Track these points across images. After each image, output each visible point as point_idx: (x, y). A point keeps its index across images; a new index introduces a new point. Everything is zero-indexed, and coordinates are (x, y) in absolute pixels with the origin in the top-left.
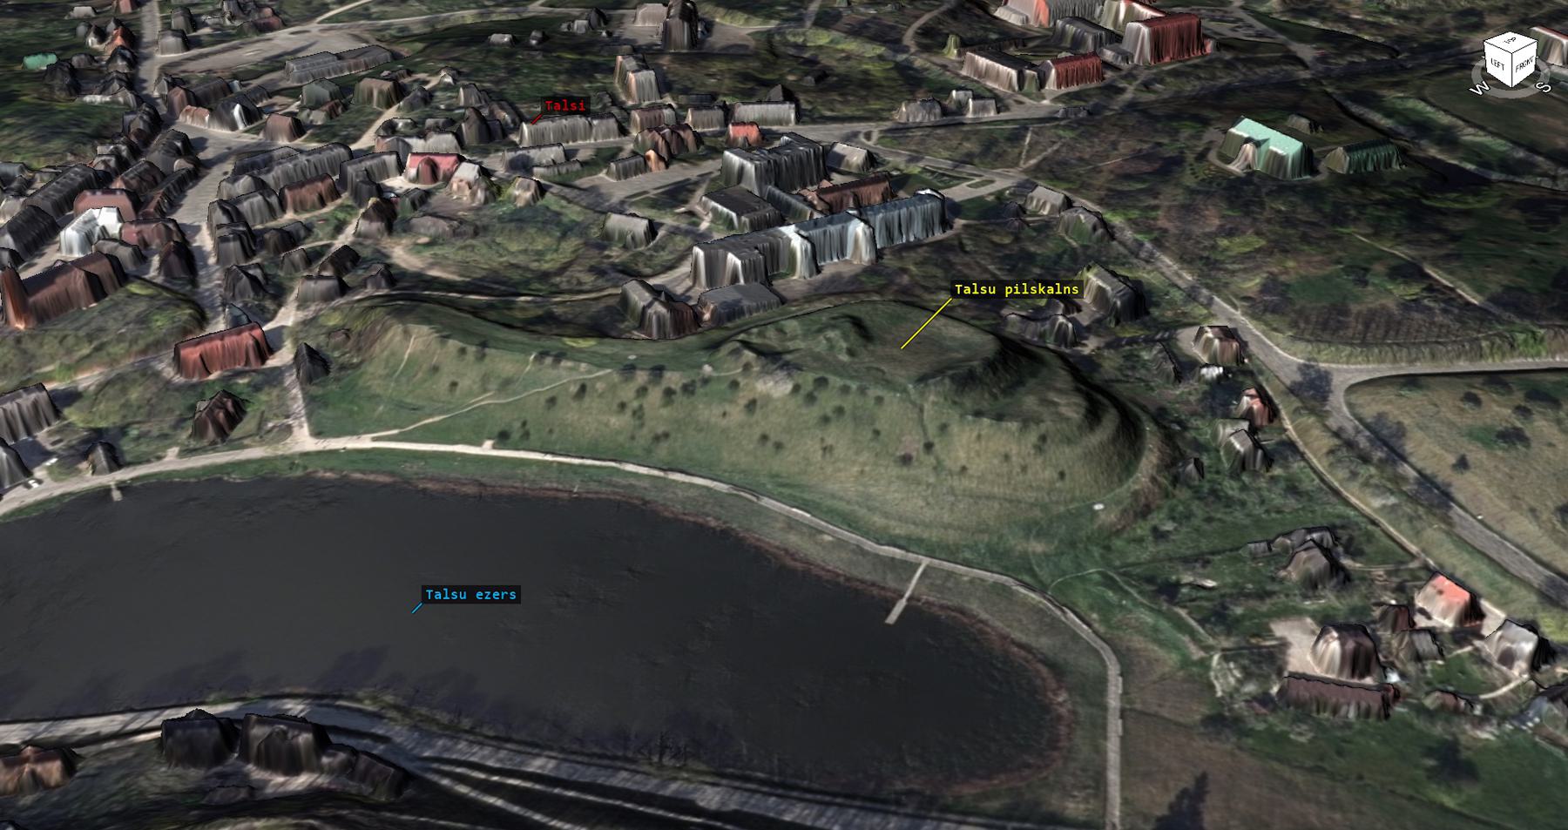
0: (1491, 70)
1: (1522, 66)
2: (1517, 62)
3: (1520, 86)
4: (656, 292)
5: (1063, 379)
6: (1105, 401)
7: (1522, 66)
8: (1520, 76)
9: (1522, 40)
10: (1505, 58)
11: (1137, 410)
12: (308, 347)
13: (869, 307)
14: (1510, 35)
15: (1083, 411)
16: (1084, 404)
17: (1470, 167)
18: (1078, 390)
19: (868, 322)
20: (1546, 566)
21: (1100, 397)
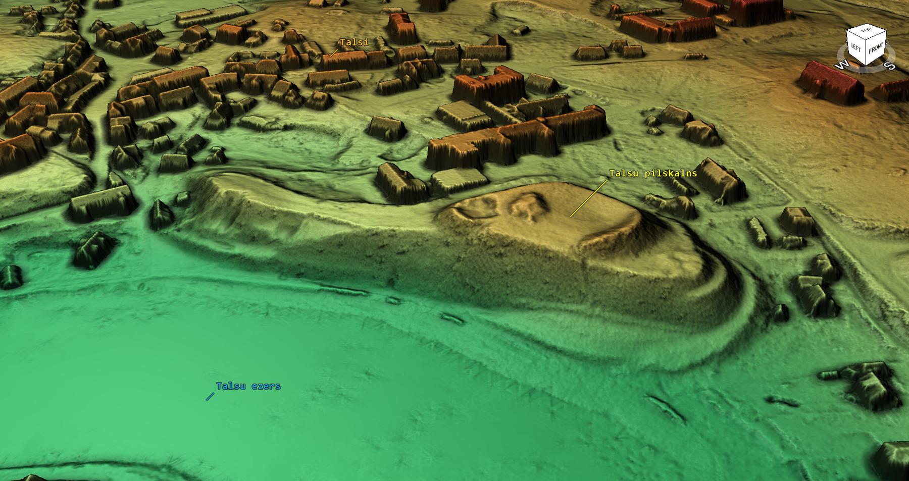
0: (852, 52)
1: (874, 49)
2: (869, 47)
3: (873, 64)
4: (125, 150)
5: (687, 243)
6: (717, 260)
7: (874, 49)
8: (870, 59)
9: (875, 30)
10: (860, 43)
11: (740, 268)
12: (161, 203)
13: (549, 185)
14: (867, 26)
15: (700, 267)
16: (701, 262)
17: (490, 104)
18: (697, 251)
19: (547, 196)
20: (35, 294)
21: (713, 257)
